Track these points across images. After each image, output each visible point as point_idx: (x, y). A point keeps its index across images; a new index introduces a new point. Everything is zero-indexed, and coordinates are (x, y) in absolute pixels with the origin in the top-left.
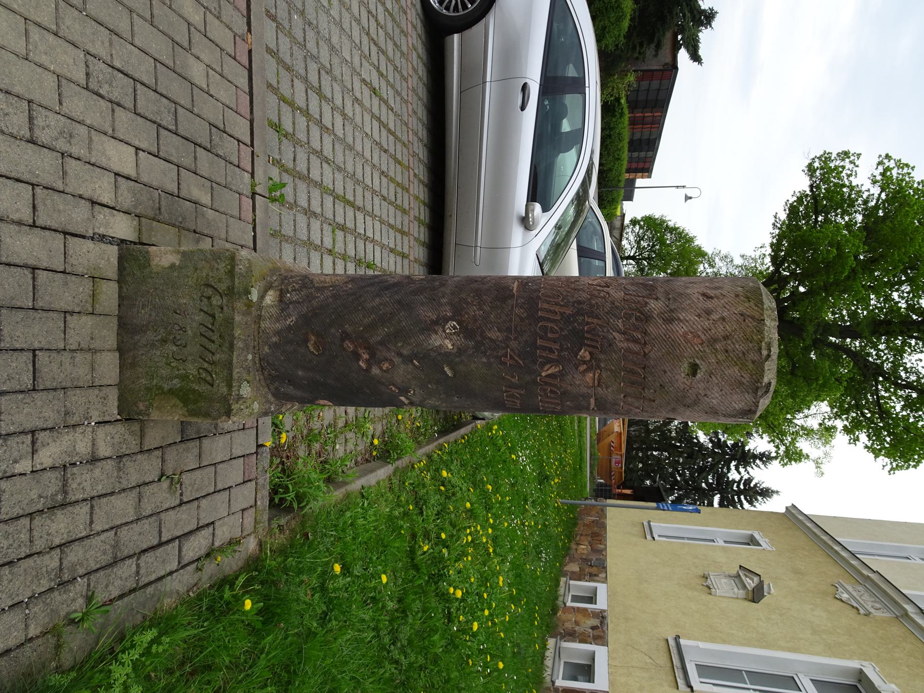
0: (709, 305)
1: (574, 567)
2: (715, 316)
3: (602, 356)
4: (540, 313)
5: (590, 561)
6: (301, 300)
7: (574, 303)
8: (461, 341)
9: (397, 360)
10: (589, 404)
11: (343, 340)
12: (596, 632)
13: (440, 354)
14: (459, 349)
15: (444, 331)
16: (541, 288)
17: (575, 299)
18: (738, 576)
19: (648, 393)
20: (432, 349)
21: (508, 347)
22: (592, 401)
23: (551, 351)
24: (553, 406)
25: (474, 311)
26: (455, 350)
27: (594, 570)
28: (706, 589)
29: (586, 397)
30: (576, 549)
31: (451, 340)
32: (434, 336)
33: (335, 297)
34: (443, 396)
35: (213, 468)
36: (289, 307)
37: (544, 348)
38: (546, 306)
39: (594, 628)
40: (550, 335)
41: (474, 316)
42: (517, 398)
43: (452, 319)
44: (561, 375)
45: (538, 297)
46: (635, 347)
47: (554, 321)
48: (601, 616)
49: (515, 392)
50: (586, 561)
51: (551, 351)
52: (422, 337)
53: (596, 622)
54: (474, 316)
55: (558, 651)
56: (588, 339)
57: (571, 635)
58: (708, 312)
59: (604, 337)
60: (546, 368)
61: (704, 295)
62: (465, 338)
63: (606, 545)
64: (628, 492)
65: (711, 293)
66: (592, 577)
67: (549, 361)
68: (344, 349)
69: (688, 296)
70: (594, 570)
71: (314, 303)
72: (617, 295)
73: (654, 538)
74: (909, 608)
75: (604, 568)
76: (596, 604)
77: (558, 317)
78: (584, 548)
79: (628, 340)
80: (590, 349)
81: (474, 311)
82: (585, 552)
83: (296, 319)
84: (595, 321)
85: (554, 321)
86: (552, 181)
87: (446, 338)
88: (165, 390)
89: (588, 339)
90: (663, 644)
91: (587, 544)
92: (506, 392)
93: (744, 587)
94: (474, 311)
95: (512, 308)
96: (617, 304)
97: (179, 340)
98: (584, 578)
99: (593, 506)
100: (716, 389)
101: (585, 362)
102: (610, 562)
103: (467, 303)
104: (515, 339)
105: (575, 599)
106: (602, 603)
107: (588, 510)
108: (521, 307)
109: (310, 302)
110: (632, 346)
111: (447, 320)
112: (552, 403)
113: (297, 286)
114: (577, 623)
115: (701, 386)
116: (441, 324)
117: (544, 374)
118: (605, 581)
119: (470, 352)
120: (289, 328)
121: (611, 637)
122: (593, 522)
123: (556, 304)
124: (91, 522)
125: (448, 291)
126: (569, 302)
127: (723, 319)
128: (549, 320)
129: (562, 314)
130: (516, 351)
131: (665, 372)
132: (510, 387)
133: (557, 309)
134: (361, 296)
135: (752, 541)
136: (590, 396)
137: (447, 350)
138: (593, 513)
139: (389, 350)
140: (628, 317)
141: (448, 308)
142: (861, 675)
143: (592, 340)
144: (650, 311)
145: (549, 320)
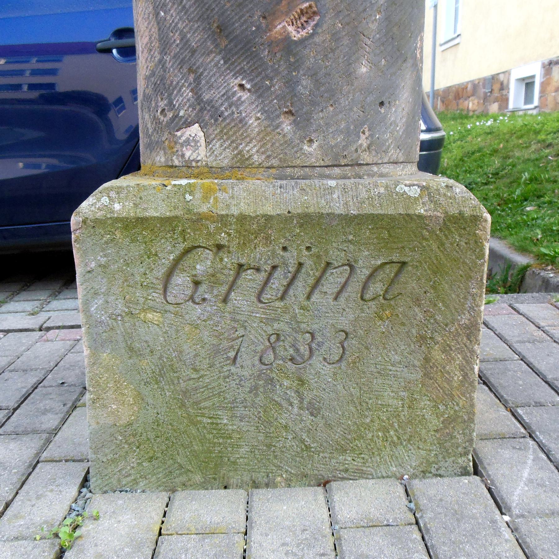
6: (191, 78)
30: (474, 111)
35: (414, 521)
36: (210, 102)
63: (468, 83)
66: (503, 87)
70: (496, 87)
75: (494, 78)
76: (533, 77)
82: (476, 102)
83: (235, 76)
86: (41, 290)
88: (516, 150)
91: (466, 102)
97: (297, 350)
98: (506, 95)
102: (486, 72)
105: (528, 99)
109: (193, 52)
118: (507, 73)
122: (443, 102)
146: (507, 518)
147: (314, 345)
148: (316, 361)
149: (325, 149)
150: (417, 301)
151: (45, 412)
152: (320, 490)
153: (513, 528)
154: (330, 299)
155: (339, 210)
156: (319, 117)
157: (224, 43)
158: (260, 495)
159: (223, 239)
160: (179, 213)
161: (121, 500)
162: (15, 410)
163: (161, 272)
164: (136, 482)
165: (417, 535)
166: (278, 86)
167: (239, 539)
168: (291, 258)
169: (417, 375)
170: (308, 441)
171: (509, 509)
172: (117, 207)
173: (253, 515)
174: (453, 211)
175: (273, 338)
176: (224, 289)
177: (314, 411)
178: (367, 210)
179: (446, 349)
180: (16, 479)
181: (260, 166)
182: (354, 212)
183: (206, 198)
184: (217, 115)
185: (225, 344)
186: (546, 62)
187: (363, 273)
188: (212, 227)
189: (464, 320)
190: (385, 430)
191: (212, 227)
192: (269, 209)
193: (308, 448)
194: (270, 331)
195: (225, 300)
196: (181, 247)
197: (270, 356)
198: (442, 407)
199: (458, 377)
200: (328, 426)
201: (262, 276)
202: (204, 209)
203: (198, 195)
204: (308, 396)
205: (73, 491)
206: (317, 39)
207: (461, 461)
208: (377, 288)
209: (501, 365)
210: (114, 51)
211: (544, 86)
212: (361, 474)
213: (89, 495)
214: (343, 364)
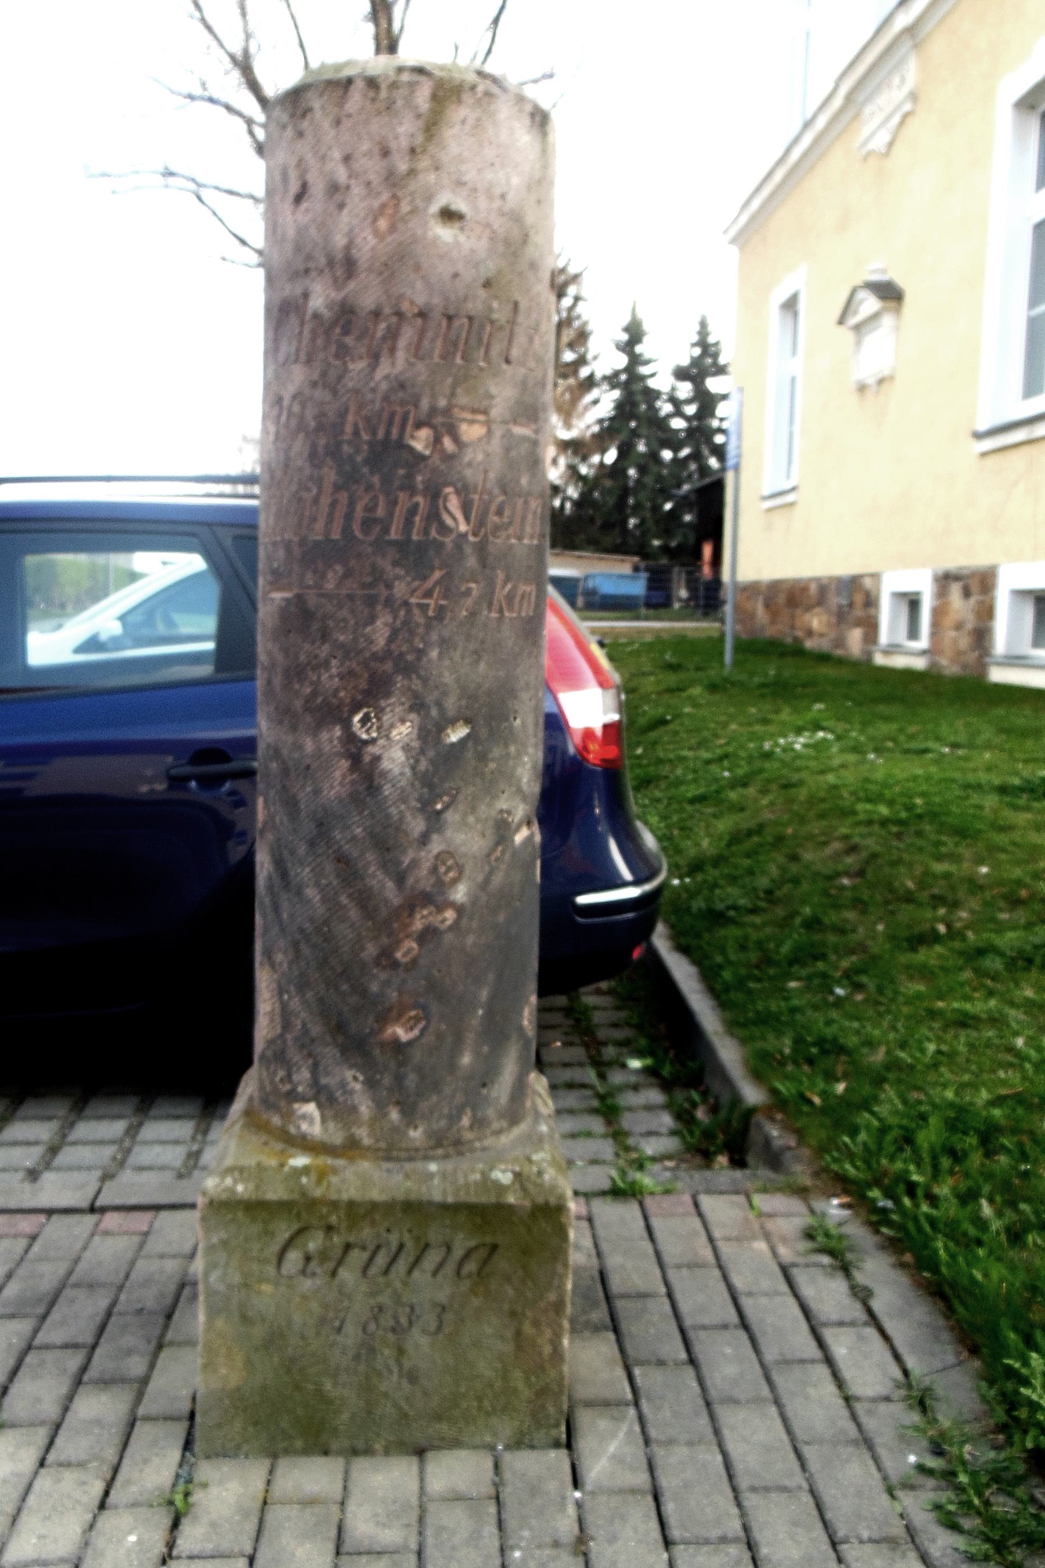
0: (317, 188)
1: (855, 637)
2: (341, 174)
3: (425, 404)
4: (336, 536)
5: (840, 607)
6: (310, 1061)
7: (314, 466)
8: (394, 706)
9: (436, 845)
10: (524, 439)
11: (395, 965)
12: (975, 587)
13: (422, 751)
14: (412, 709)
15: (373, 741)
16: (282, 541)
17: (307, 465)
18: (858, 328)
19: (501, 315)
20: (413, 768)
21: (406, 604)
22: (518, 430)
23: (413, 510)
24: (530, 517)
25: (330, 679)
26: (413, 716)
27: (859, 599)
28: (885, 386)
29: (510, 443)
31: (392, 726)
32: (385, 764)
33: (302, 986)
34: (512, 749)
37: (409, 523)
38: (319, 526)
39: (967, 593)
40: (380, 512)
41: (342, 677)
42: (515, 588)
43: (347, 724)
44: (464, 491)
45: (303, 542)
46: (407, 335)
47: (352, 504)
48: (945, 580)
49: (501, 592)
50: (842, 617)
51: (413, 510)
52: (387, 790)
53: (955, 590)
54: (342, 677)
55: (1015, 661)
56: (388, 433)
57: (982, 636)
58: (334, 188)
59: (386, 398)
60: (449, 521)
61: (299, 198)
62: (388, 695)
64: (707, 550)
65: (294, 188)
66: (871, 602)
67: (434, 516)
68: (414, 962)
69: (301, 231)
70: (859, 599)
71: (316, 1029)
72: (298, 375)
73: (793, 489)
74: (903, 20)
77: (343, 497)
78: (816, 621)
79: (392, 350)
80: (409, 428)
81: (331, 677)
84: (350, 418)
85: (352, 504)
87: (388, 737)
89: (388, 433)
90: (991, 462)
92: (501, 611)
93: (875, 316)
94: (330, 679)
95: (322, 595)
96: (315, 376)
97: (398, 1322)
99: (737, 608)
100: (489, 175)
101: (437, 440)
102: (843, 569)
103: (315, 694)
104: (389, 586)
105: (913, 633)
106: (924, 585)
107: (744, 616)
108: (323, 576)
109: (313, 1040)
110: (402, 343)
111: (350, 737)
112: (524, 518)
113: (281, 1073)
114: (959, 626)
115: (483, 203)
116: (360, 749)
117: (463, 527)
118: (876, 576)
119: (417, 685)
120: (371, 1084)
121: (978, 560)
122: (767, 606)
123: (316, 501)
124: (784, 1489)
125: (290, 739)
126: (311, 478)
127: (347, 159)
128: (349, 517)
129: (337, 488)
130: (416, 583)
131: (456, 275)
132: (490, 605)
133: (325, 501)
134: (302, 931)
135: (790, 305)
136: (508, 435)
137: (414, 736)
138: (749, 606)
139: (415, 863)
140: (343, 352)
141: (324, 736)
142: (1027, 103)
143: (390, 424)
144: (329, 306)
145: (349, 517)
146: (578, 1494)
147: (414, 1318)
148: (415, 1331)
149: (429, 1134)
150: (508, 1279)
151: (129, 1352)
152: (415, 1460)
153: (579, 1505)
154: (429, 1275)
155: (437, 1196)
156: (424, 1106)
157: (340, 1039)
158: (360, 1464)
159: (333, 1219)
160: (296, 1196)
161: (226, 1467)
162: (94, 1347)
163: (276, 1247)
164: (238, 1447)
165: (493, 1510)
166: (387, 1080)
167: (335, 1509)
168: (394, 1239)
169: (508, 1348)
170: (405, 1407)
171: (583, 1485)
172: (240, 1188)
173: (351, 1486)
174: (540, 1200)
175: (376, 1310)
176: (331, 1265)
177: (413, 1378)
178: (463, 1197)
179: (536, 1324)
180: (117, 1440)
181: (369, 1148)
182: (450, 1200)
183: (319, 1181)
184: (331, 1099)
185: (331, 1315)
186: (940, 572)
187: (458, 1253)
188: (324, 1210)
189: (552, 1297)
190: (479, 1399)
191: (324, 1210)
192: (376, 1195)
193: (406, 1416)
194: (372, 1302)
195: (334, 1274)
196: (296, 1226)
197: (372, 1327)
198: (533, 1379)
199: (547, 1350)
200: (426, 1394)
201: (365, 1256)
202: (318, 1193)
203: (313, 1177)
204: (407, 1364)
205: (175, 1455)
206: (424, 1040)
207: (554, 1432)
208: (471, 1267)
209: (639, 1304)
210: (193, 784)
211: (938, 614)
212: (456, 1444)
213: (193, 1460)
214: (441, 1336)
